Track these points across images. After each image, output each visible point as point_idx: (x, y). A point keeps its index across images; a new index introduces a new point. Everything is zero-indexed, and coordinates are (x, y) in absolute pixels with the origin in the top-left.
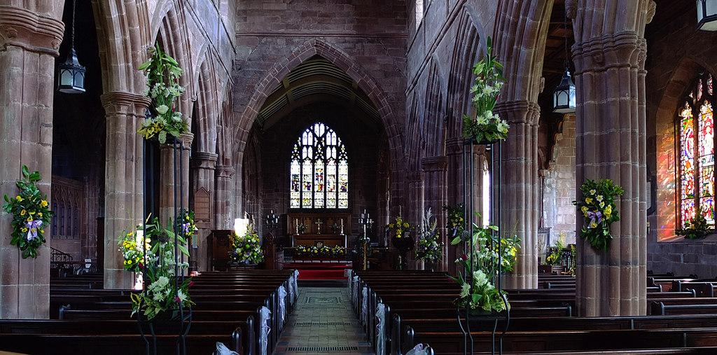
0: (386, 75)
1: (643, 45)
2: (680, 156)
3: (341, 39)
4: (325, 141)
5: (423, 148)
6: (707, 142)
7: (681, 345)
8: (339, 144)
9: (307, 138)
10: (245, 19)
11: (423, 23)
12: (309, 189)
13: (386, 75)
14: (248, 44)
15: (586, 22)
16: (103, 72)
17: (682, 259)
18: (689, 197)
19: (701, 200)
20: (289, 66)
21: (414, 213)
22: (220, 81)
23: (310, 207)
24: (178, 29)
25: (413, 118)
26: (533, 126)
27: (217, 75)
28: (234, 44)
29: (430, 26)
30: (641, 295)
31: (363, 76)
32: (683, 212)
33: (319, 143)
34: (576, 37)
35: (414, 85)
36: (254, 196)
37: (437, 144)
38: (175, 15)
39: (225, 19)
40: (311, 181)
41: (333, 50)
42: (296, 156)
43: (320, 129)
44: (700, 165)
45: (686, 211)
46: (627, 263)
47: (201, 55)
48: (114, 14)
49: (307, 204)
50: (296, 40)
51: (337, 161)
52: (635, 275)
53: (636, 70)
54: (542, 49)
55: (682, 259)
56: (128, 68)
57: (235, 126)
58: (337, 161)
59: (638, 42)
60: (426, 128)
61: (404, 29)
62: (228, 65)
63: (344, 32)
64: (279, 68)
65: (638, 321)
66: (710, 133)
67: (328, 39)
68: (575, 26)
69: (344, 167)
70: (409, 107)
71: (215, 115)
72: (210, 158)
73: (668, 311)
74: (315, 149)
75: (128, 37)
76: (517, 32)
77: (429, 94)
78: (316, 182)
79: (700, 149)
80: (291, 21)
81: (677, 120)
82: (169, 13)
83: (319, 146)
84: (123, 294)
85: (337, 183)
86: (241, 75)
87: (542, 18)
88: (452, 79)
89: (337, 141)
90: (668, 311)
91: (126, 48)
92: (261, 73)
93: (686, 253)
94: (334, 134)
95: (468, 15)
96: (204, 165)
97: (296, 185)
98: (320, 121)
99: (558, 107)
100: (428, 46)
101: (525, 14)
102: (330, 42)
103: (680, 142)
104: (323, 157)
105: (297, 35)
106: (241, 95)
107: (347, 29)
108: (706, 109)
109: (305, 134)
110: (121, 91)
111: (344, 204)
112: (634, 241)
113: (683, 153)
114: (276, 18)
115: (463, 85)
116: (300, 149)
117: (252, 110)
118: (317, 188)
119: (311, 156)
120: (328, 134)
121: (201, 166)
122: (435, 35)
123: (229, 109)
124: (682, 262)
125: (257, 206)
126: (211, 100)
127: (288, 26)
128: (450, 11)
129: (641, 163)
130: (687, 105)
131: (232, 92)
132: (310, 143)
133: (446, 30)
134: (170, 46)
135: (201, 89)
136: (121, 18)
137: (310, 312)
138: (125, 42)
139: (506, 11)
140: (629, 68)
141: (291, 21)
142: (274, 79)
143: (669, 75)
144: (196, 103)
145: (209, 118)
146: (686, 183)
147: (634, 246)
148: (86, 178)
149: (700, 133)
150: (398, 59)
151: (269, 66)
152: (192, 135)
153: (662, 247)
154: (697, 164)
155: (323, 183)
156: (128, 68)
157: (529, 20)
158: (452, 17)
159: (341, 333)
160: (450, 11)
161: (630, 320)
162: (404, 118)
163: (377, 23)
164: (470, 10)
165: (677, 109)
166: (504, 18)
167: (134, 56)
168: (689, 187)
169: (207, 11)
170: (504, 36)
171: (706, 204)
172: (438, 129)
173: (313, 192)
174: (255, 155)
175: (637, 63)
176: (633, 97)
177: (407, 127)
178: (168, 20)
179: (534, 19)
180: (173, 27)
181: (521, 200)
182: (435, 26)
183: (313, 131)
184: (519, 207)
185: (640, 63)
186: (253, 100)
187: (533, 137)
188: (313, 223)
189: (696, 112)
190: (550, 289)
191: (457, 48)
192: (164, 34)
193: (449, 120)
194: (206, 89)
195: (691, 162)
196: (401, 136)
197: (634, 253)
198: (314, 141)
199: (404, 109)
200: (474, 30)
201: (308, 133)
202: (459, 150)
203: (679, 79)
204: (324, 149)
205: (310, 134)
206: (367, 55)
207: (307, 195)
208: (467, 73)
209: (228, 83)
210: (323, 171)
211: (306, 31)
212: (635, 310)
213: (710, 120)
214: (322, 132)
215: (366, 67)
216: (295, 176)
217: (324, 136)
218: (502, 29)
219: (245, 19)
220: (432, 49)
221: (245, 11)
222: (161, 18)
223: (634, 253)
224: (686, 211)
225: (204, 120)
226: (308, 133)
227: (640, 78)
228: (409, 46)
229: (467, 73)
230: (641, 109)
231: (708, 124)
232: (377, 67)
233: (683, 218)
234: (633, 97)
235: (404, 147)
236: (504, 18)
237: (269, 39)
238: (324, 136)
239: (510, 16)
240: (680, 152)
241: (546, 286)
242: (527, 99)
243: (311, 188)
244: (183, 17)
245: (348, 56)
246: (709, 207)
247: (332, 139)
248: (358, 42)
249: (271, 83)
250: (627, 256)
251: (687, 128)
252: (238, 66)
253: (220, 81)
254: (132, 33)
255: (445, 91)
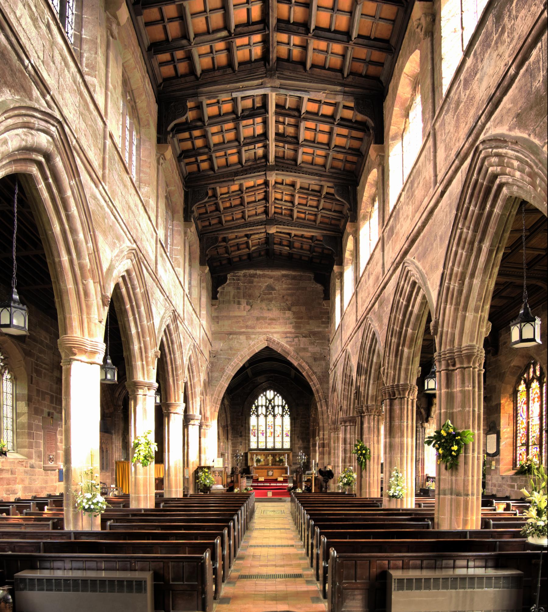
0: (315, 359)
1: (481, 352)
2: (517, 417)
3: (284, 335)
4: (274, 402)
5: (341, 410)
6: (535, 408)
7: (494, 551)
8: (284, 404)
9: (261, 400)
10: (218, 323)
11: (341, 325)
12: (263, 435)
13: (315, 359)
14: (220, 339)
15: (444, 338)
16: (127, 367)
17: (516, 487)
18: (523, 445)
19: (530, 448)
20: (248, 354)
21: (334, 453)
22: (201, 366)
23: (264, 447)
24: (174, 336)
25: (334, 390)
26: (413, 400)
27: (199, 363)
28: (210, 340)
29: (345, 328)
30: (477, 514)
31: (299, 360)
32: (518, 455)
33: (270, 403)
34: (437, 348)
35: (335, 367)
36: (226, 441)
37: (350, 408)
38: (171, 327)
39: (204, 323)
40: (264, 430)
41: (278, 343)
42: (253, 413)
43: (270, 394)
44: (530, 423)
45: (520, 454)
46: (467, 495)
47: (189, 351)
48: (133, 331)
49: (262, 446)
50: (253, 336)
51: (282, 416)
52: (472, 502)
53: (476, 370)
54: (419, 348)
55: (516, 487)
56: (143, 365)
57: (212, 395)
58: (282, 416)
59: (478, 351)
60: (342, 397)
61: (327, 327)
62: (207, 355)
63: (286, 330)
64: (241, 356)
65: (473, 533)
66: (538, 402)
67: (275, 335)
68: (437, 341)
69: (287, 419)
70: (331, 382)
71: (198, 389)
72: (196, 418)
73: (496, 526)
74: (267, 408)
75: (142, 345)
76: (402, 339)
77: (345, 375)
78: (268, 430)
79: (530, 413)
80: (249, 323)
81: (515, 392)
82: (168, 326)
83: (270, 406)
84: (143, 512)
85: (283, 430)
86: (216, 361)
87: (419, 328)
88: (359, 366)
89: (283, 402)
90: (496, 526)
91: (141, 352)
92: (229, 359)
93: (518, 483)
94: (280, 398)
95: (370, 324)
96: (192, 422)
97: (254, 433)
98: (270, 388)
99: (428, 390)
100: (344, 341)
101: (407, 326)
102: (276, 338)
103: (517, 408)
104: (272, 413)
105: (254, 333)
106: (215, 374)
107: (289, 328)
108: (535, 385)
109: (260, 398)
110: (139, 380)
111: (287, 445)
112: (473, 481)
113: (519, 415)
114: (239, 322)
115: (367, 370)
116: (257, 408)
117: (224, 384)
118: (268, 434)
119: (264, 413)
120: (276, 397)
121: (190, 423)
122: (348, 334)
123: (209, 384)
124: (516, 489)
125: (228, 447)
126: (196, 379)
127: (247, 327)
128: (358, 319)
129: (479, 429)
130: (522, 382)
131: (210, 373)
132: (264, 404)
133: (355, 332)
134: (169, 347)
135: (189, 373)
136: (138, 333)
137: (263, 520)
138: (140, 348)
139: (394, 324)
140: (471, 369)
141: (249, 323)
142: (238, 363)
143: (510, 362)
144: (186, 384)
145: (195, 392)
146: (520, 435)
147: (473, 484)
148: (113, 431)
149: (531, 402)
150: (324, 349)
151: (234, 354)
152: (184, 405)
153: (503, 478)
154: (528, 423)
155: (272, 430)
156: (143, 365)
157: (410, 331)
158: (359, 324)
159: (284, 535)
160: (358, 319)
161: (466, 532)
162: (328, 389)
163: (309, 324)
164: (372, 321)
165: (516, 385)
166: (393, 328)
167: (147, 357)
168: (523, 438)
169: (192, 321)
170: (393, 341)
171: (533, 450)
172: (350, 398)
173: (266, 437)
174: (226, 412)
175: (477, 365)
176: (474, 387)
177: (330, 395)
178: (168, 331)
179: (414, 329)
180: (171, 335)
181: (403, 449)
182: (348, 328)
183: (265, 396)
184: (402, 453)
185: (480, 365)
186: (224, 377)
187: (413, 407)
188: (266, 457)
189: (528, 387)
190: (422, 508)
191: (362, 348)
192: (164, 339)
193: (358, 393)
194: (193, 372)
195: (525, 421)
196: (326, 401)
197: (473, 488)
198: (266, 402)
199: (328, 382)
200: (374, 334)
201: (262, 397)
202: (364, 413)
203: (517, 365)
204: (273, 408)
205: (264, 398)
206: (302, 346)
207: (262, 439)
208: (370, 363)
209: (207, 367)
210: (273, 423)
211: (260, 330)
212: (472, 525)
213: (537, 394)
214: (272, 396)
215: (302, 354)
216: (254, 426)
217: (274, 398)
218: (392, 336)
219: (218, 323)
220: (346, 344)
221: (217, 317)
222: (163, 330)
223: (473, 488)
224: (520, 454)
225: (192, 393)
226: (262, 397)
227: (479, 375)
228: (331, 340)
229: (370, 363)
230: (479, 395)
231: (536, 396)
232: (309, 354)
233: (518, 459)
234: (474, 387)
235: (328, 408)
236: (393, 328)
237: (235, 336)
238: (274, 398)
239: (484, 179)
240: (517, 414)
241: (420, 505)
242: (408, 382)
243: (265, 434)
244: (177, 327)
245: (288, 347)
246: (535, 452)
247: (279, 400)
248: (297, 337)
249: (236, 366)
250: (468, 490)
251: (522, 398)
252: (214, 355)
253: (201, 366)
254: (145, 342)
255: (354, 374)
